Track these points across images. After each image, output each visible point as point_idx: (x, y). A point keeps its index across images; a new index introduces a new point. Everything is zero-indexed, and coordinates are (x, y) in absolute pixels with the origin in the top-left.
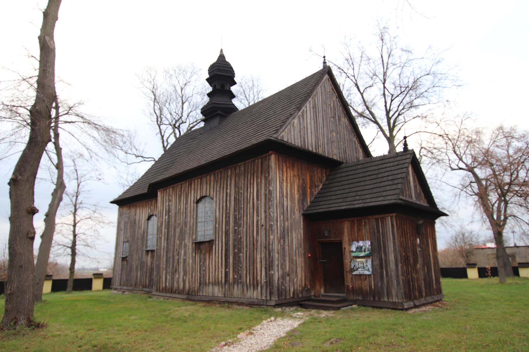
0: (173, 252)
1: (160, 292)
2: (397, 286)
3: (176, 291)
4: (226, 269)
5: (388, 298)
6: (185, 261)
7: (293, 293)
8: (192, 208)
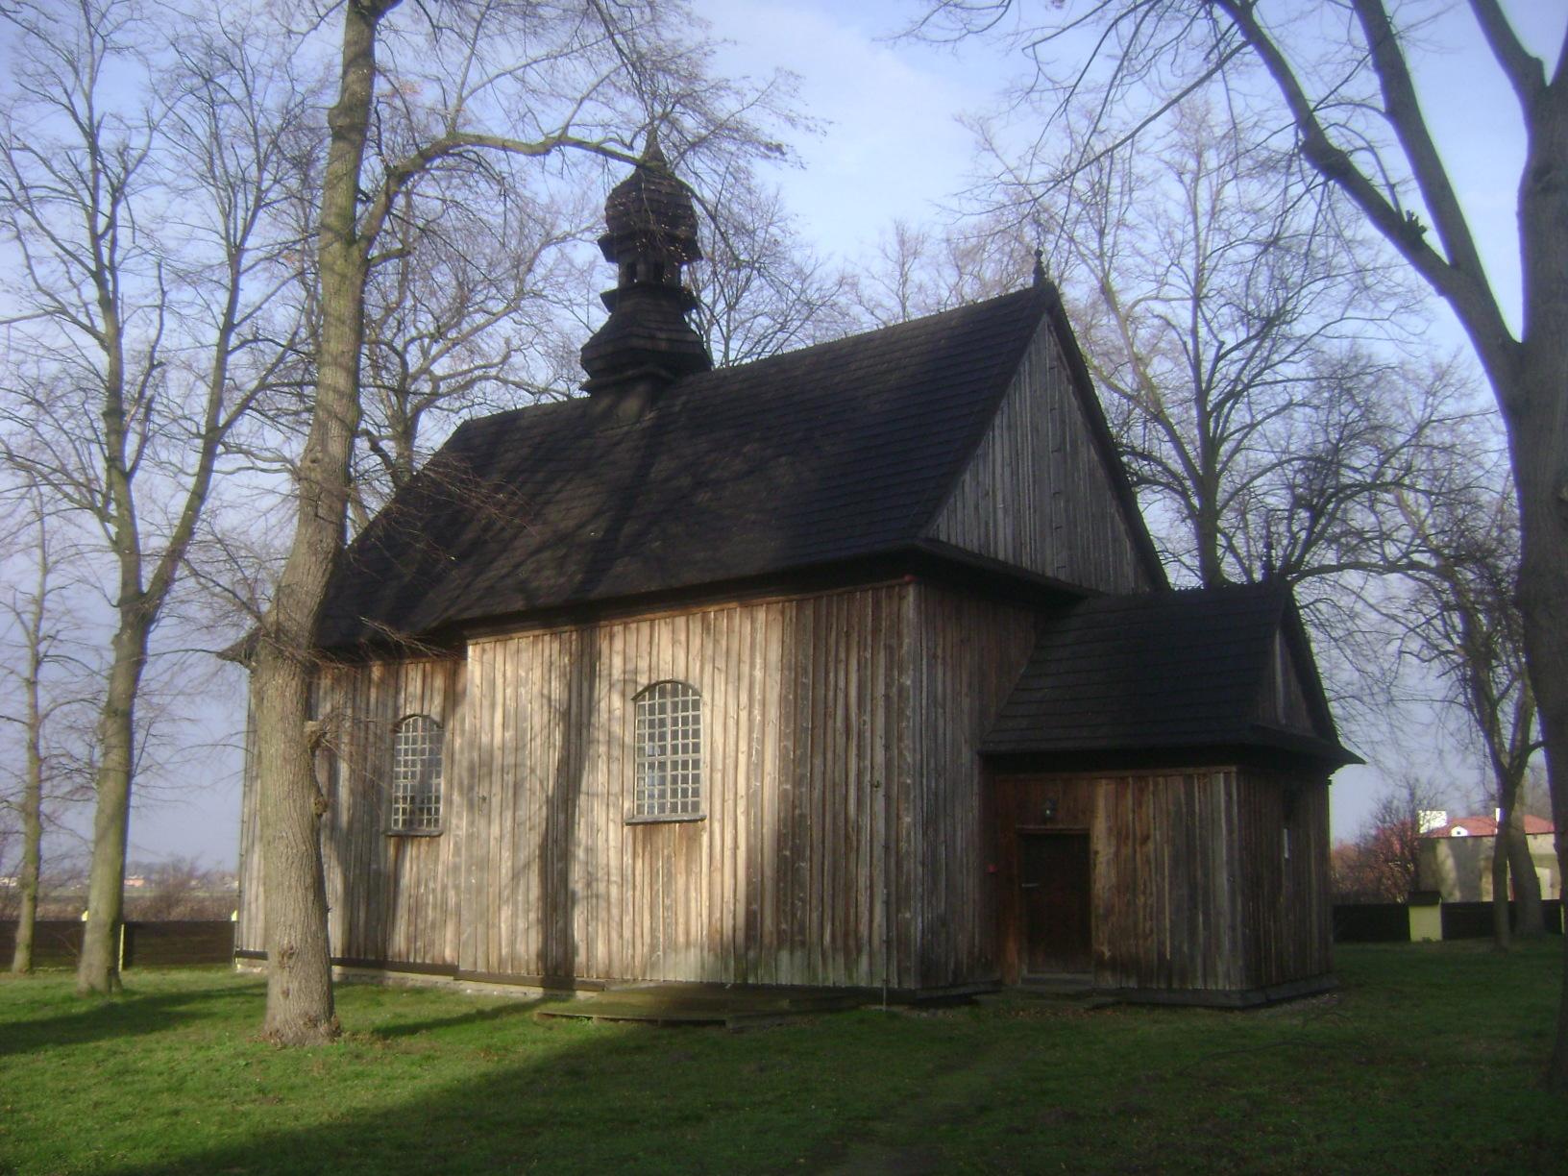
5: (1205, 982)
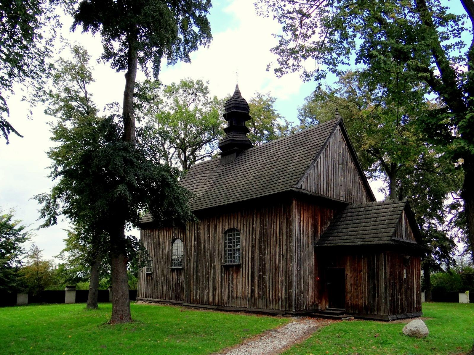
0: (203, 272)
1: (191, 303)
2: (385, 304)
3: (206, 302)
4: (252, 286)
6: (214, 279)
7: (306, 307)
8: (221, 237)
